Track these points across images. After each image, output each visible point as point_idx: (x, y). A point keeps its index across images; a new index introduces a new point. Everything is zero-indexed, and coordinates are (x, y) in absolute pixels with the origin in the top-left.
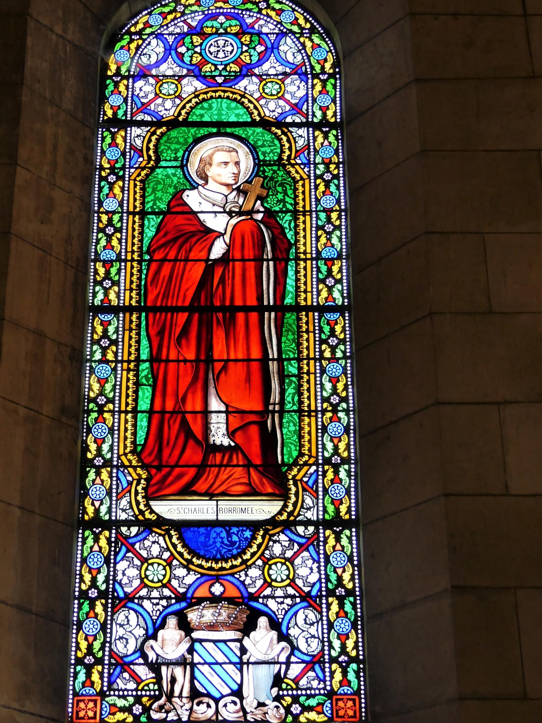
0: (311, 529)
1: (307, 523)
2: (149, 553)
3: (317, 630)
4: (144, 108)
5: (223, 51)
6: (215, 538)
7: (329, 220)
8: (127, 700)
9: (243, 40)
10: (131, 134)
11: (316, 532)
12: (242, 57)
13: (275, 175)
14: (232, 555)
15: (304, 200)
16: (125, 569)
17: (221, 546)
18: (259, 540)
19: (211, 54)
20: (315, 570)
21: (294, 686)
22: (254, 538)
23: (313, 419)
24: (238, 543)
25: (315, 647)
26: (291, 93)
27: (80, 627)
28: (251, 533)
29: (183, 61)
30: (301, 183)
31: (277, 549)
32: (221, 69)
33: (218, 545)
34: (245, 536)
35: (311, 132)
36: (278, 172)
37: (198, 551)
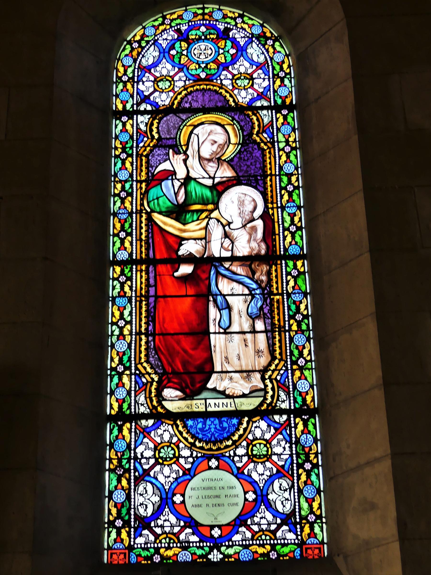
0: (285, 417)
1: (281, 412)
2: (162, 439)
3: (290, 494)
4: (146, 99)
5: (204, 53)
6: (210, 425)
7: (290, 182)
8: (149, 551)
9: (219, 45)
10: (134, 502)
11: (289, 419)
12: (219, 58)
13: (249, 169)
14: (223, 437)
15: (277, 282)
16: (143, 452)
17: (215, 431)
18: (245, 425)
19: (195, 55)
20: (287, 449)
21: (273, 537)
22: (240, 423)
23: (279, 266)
24: (227, 429)
25: (288, 508)
26: (277, 454)
27: (110, 497)
28: (237, 421)
29: (173, 61)
30: (268, 151)
31: (258, 433)
32: (203, 67)
33: (213, 430)
34: (233, 423)
35: (274, 114)
36: (251, 166)
37: (197, 435)
